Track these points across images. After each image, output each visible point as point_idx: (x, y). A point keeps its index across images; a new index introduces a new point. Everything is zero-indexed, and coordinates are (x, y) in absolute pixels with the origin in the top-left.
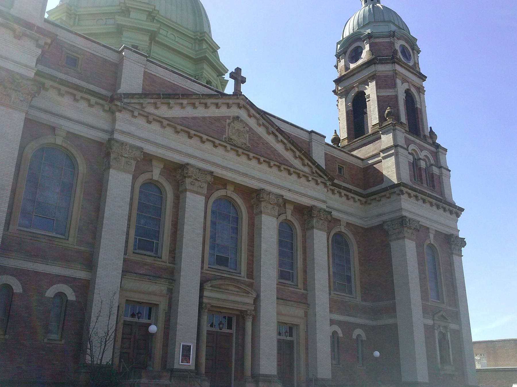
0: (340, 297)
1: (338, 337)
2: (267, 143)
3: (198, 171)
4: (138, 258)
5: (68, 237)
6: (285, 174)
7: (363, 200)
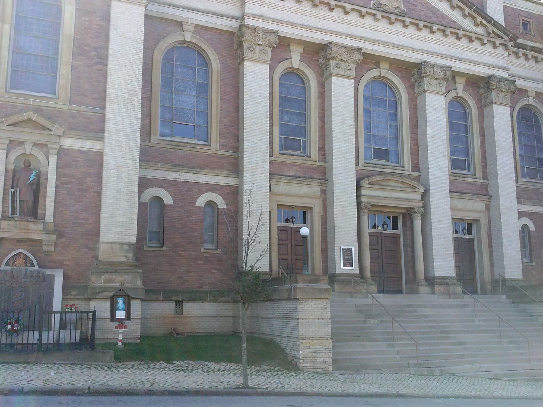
1: (218, 209)
3: (343, 49)
6: (452, 39)
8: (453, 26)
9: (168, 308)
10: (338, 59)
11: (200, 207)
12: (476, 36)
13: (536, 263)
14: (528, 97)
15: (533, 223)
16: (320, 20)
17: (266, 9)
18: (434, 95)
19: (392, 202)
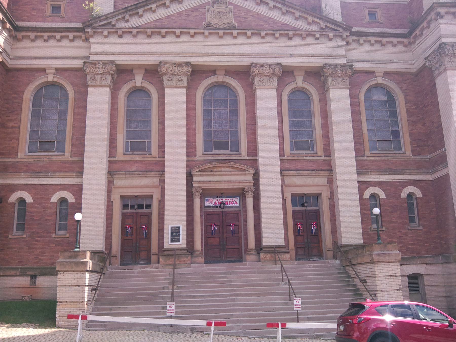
0: (378, 155)
1: (380, 199)
2: (258, 14)
3: (173, 66)
4: (128, 158)
5: (405, 151)
6: (284, 40)
7: (406, 41)
8: (286, 28)
9: (25, 281)
10: (169, 74)
11: (53, 203)
13: (386, 228)
14: (376, 77)
15: (384, 191)
16: (154, 46)
17: (108, 46)
18: (266, 90)
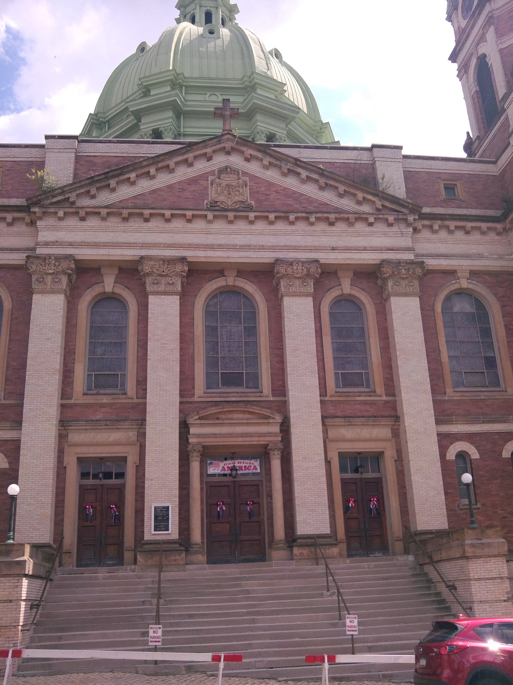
1: (471, 460)
2: (285, 189)
3: (161, 263)
7: (499, 226)
10: (154, 274)
12: (356, 216)
14: (459, 279)
15: (476, 447)
16: (133, 234)
17: (64, 233)
19: (235, 439)
